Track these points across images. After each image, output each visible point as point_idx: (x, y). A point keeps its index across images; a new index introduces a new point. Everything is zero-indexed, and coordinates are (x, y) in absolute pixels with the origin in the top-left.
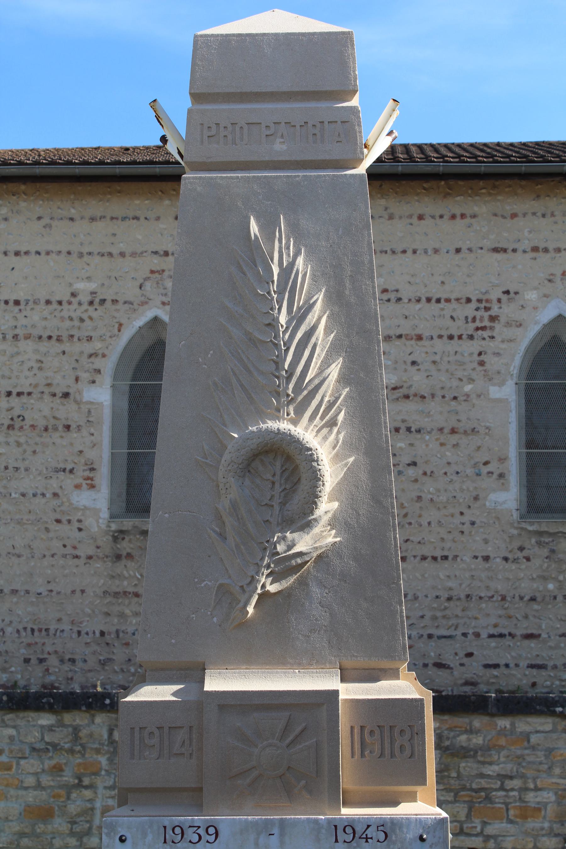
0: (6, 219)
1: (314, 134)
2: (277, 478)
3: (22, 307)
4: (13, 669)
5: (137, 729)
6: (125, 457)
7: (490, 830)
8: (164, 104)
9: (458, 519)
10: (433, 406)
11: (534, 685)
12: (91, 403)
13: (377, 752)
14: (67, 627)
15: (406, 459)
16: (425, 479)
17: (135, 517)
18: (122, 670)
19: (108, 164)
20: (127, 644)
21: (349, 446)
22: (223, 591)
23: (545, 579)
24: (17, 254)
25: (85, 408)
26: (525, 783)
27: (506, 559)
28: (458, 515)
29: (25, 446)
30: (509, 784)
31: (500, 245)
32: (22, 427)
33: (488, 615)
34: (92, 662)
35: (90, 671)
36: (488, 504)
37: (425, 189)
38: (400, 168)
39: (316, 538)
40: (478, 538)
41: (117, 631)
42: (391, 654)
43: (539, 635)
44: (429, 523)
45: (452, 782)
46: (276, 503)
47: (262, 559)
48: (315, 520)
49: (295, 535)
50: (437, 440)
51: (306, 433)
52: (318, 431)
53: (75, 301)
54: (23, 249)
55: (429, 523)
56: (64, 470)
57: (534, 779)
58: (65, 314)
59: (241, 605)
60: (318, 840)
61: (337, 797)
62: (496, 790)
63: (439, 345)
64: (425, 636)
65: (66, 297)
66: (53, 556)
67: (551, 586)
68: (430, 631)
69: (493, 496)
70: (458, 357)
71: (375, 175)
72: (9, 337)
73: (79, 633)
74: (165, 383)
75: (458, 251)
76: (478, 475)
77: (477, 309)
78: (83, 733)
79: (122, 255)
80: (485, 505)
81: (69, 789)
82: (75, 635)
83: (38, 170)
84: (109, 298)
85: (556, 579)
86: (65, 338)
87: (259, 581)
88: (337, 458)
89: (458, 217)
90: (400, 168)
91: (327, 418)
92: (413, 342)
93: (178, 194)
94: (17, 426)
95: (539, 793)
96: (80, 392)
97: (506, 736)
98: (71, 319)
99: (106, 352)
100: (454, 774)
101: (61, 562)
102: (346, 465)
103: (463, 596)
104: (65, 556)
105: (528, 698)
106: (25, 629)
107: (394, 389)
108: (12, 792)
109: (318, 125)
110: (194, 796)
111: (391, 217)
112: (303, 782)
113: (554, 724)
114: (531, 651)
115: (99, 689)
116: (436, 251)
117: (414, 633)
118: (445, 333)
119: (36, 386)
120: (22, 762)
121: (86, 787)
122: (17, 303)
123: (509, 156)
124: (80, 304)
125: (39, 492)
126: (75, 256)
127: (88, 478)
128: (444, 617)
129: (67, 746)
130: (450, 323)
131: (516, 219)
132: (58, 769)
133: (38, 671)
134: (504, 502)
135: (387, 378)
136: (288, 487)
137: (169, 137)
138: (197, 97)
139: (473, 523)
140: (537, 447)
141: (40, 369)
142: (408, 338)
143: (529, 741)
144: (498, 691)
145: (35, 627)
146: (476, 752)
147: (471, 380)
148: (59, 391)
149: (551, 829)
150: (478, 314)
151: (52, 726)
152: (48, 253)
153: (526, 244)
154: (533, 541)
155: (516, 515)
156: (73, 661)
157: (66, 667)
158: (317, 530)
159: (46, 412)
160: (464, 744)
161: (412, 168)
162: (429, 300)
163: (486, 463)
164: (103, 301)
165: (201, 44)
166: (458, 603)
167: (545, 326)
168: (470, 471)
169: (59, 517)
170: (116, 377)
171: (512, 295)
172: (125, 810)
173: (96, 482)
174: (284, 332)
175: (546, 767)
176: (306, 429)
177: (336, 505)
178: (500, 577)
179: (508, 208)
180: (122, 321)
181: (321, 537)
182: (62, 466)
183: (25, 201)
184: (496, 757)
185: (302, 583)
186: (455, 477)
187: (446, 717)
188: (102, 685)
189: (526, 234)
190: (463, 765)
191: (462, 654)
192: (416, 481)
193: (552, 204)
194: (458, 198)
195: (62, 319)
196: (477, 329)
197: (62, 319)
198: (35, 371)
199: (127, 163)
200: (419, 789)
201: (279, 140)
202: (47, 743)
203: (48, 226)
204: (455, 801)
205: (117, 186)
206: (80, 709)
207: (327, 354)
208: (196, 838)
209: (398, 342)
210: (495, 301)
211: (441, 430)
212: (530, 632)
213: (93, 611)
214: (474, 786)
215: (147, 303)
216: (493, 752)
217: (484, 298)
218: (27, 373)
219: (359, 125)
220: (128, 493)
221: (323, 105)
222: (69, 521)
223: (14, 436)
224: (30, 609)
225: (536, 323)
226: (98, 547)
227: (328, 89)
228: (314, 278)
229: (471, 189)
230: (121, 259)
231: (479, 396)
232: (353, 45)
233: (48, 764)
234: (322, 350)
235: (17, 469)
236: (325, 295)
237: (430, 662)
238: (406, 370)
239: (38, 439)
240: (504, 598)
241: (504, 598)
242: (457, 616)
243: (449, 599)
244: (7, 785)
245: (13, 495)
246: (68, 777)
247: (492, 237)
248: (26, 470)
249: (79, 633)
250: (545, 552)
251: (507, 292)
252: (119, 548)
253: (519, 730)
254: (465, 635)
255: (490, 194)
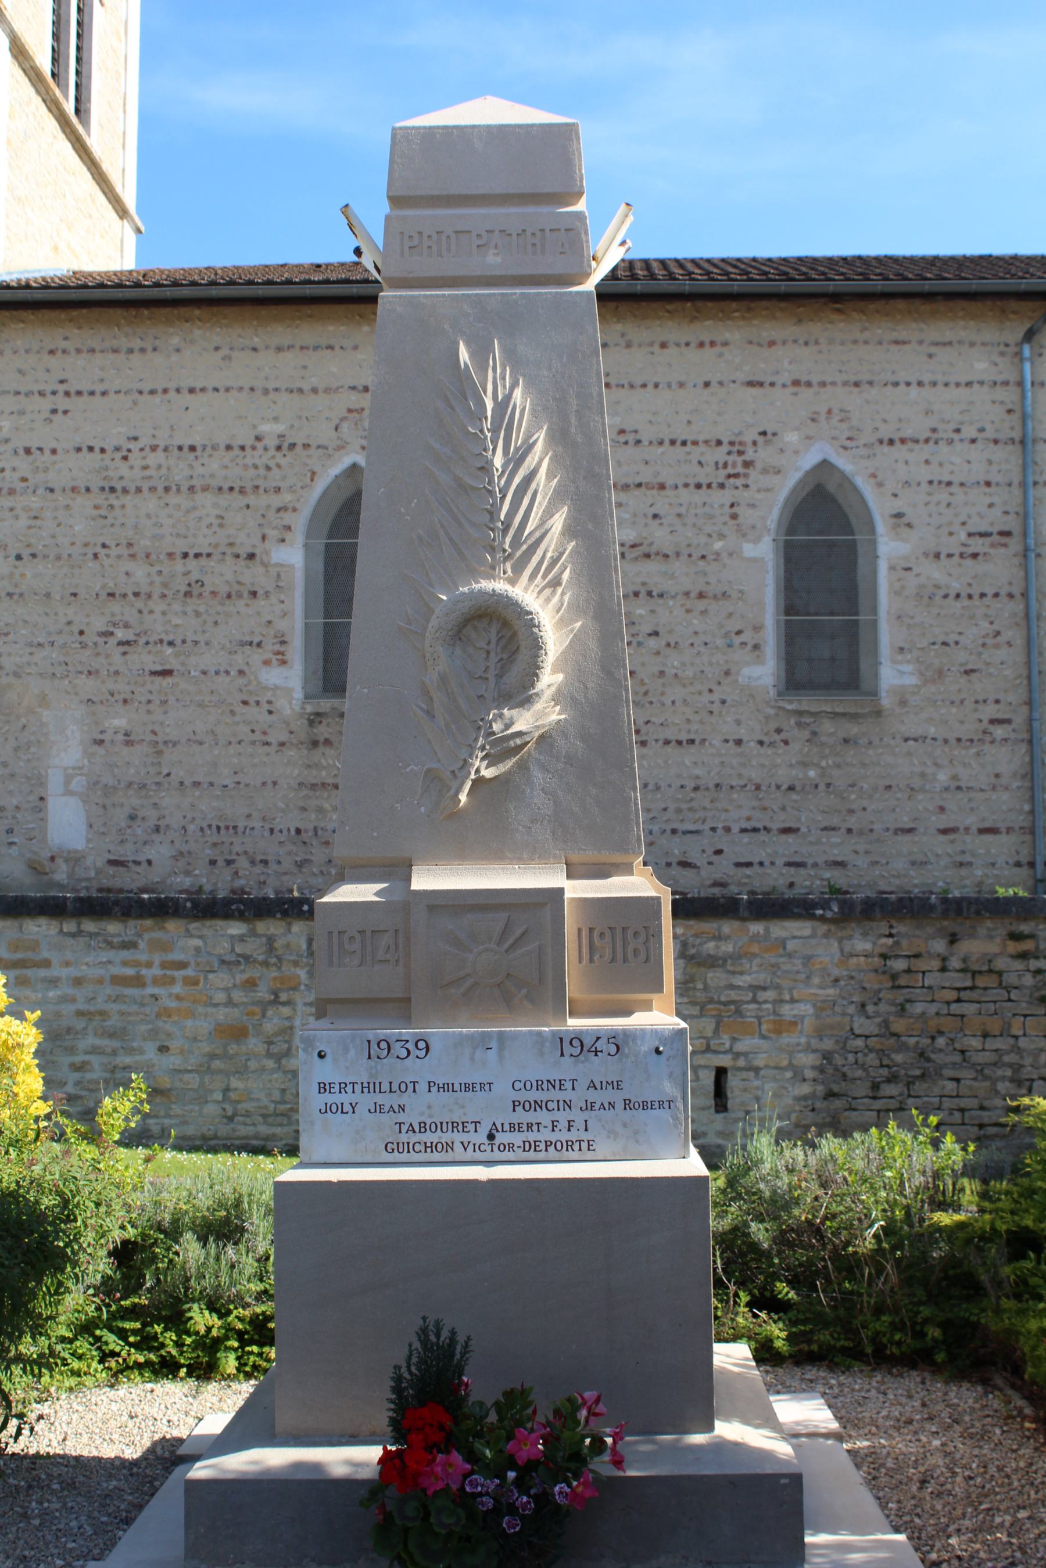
0: (178, 350)
1: (534, 245)
2: (493, 646)
3: (199, 453)
4: (197, 872)
5: (335, 935)
6: (321, 627)
7: (739, 1047)
8: (358, 210)
9: (706, 697)
10: (677, 567)
11: (791, 885)
12: (281, 565)
13: (608, 956)
14: (257, 825)
15: (647, 628)
16: (668, 651)
17: (334, 697)
18: (322, 873)
19: (296, 283)
20: (327, 843)
21: (576, 609)
22: (431, 776)
23: (804, 765)
24: (192, 391)
25: (273, 571)
26: (780, 994)
27: (761, 743)
28: (706, 693)
29: (205, 616)
30: (762, 996)
31: (756, 378)
32: (201, 595)
33: (740, 807)
34: (287, 864)
35: (285, 874)
36: (740, 679)
37: (668, 311)
38: (639, 288)
39: (539, 715)
40: (729, 719)
41: (315, 829)
42: (624, 846)
43: (798, 830)
44: (673, 702)
45: (698, 994)
46: (491, 675)
47: (476, 740)
48: (537, 694)
49: (514, 712)
50: (683, 605)
51: (526, 594)
52: (540, 592)
53: (260, 445)
54: (198, 385)
55: (673, 702)
56: (251, 643)
57: (790, 990)
58: (249, 461)
59: (452, 792)
60: (541, 1054)
61: (560, 1004)
62: (748, 1002)
63: (685, 496)
64: (669, 832)
65: (249, 442)
66: (239, 743)
67: (812, 773)
68: (674, 826)
69: (746, 671)
70: (707, 509)
71: (606, 296)
72: (184, 488)
73: (272, 831)
74: (362, 539)
75: (707, 384)
76: (730, 646)
77: (729, 453)
78: (279, 943)
79: (315, 391)
80: (737, 681)
81: (264, 1006)
82: (267, 833)
83: (214, 292)
84: (300, 442)
85: (817, 765)
86: (249, 490)
87: (472, 765)
88: (562, 623)
89: (707, 345)
90: (639, 287)
91: (550, 576)
92: (655, 492)
93: (375, 314)
94: (195, 593)
95: (796, 1005)
96: (267, 552)
97: (759, 942)
98: (256, 467)
99: (297, 506)
100: (700, 986)
101: (250, 750)
102: (572, 630)
103: (711, 786)
104: (253, 743)
105: (784, 900)
106: (210, 826)
107: (633, 546)
108: (201, 1009)
109: (538, 233)
110: (402, 1007)
111: (629, 345)
112: (524, 991)
113: (814, 929)
114: (788, 847)
115: (296, 894)
116: (681, 385)
117: (656, 828)
118: (692, 481)
119: (217, 546)
120: (211, 976)
121: (284, 1004)
122: (192, 448)
123: (766, 273)
124: (266, 449)
125: (222, 669)
126: (259, 392)
127: (279, 653)
128: (690, 809)
129: (261, 958)
130: (697, 469)
131: (774, 348)
132: (251, 984)
133: (226, 874)
134: (759, 678)
135: (619, 533)
136: (505, 656)
137: (364, 249)
138: (396, 201)
139: (723, 702)
140: (797, 614)
141: (221, 526)
142: (649, 487)
143: (785, 948)
144: (752, 893)
145: (222, 825)
146: (725, 961)
147: (722, 536)
148: (243, 552)
149: (808, 1044)
150: (730, 459)
151: (243, 935)
152: (227, 390)
153: (786, 378)
154: (792, 722)
155: (772, 692)
156: (265, 862)
157: (258, 869)
158: (538, 706)
159: (229, 576)
160: (712, 952)
161: (653, 287)
162: (673, 442)
163: (739, 633)
164: (293, 446)
165: (400, 139)
166: (707, 793)
167: (808, 473)
168: (720, 642)
169: (246, 698)
170: (309, 535)
171: (769, 436)
172: (323, 1023)
173: (288, 657)
174: (500, 477)
175: (804, 976)
176: (526, 589)
177: (560, 677)
178: (754, 763)
179: (765, 334)
180: (315, 469)
181: (543, 714)
182: (248, 638)
183: (199, 328)
184: (748, 966)
185: (522, 767)
186: (702, 649)
187: (691, 922)
188: (299, 889)
189: (786, 365)
190: (710, 975)
191: (710, 851)
192: (658, 653)
193: (815, 329)
194: (707, 323)
195: (246, 467)
196: (729, 476)
197: (246, 467)
198: (215, 528)
199: (319, 282)
200: (655, 997)
201: (492, 251)
202: (239, 955)
203: (227, 358)
204: (701, 1016)
205: (307, 310)
206: (274, 916)
207: (549, 503)
208: (404, 1053)
209: (637, 492)
210: (750, 443)
211: (687, 594)
212: (787, 825)
213: (287, 806)
214: (723, 999)
215: (343, 447)
216: (744, 961)
217: (737, 440)
218: (206, 531)
219: (586, 233)
220: (325, 670)
221: (544, 209)
222: (258, 703)
223: (192, 604)
224: (214, 804)
225: (797, 469)
226: (291, 733)
227: (549, 190)
228: (534, 412)
229: (723, 311)
230: (313, 396)
231: (731, 555)
232: (578, 139)
233: (240, 978)
234: (544, 498)
235: (196, 643)
236: (547, 434)
237: (674, 861)
238: (646, 525)
239: (220, 608)
240: (758, 787)
241: (758, 787)
242: (705, 808)
243: (696, 789)
244: (194, 1002)
245: (193, 673)
246: (263, 993)
247: (747, 368)
248: (207, 644)
249: (272, 831)
250: (806, 734)
251: (764, 433)
252: (316, 733)
253: (773, 936)
254: (713, 829)
255: (744, 318)
